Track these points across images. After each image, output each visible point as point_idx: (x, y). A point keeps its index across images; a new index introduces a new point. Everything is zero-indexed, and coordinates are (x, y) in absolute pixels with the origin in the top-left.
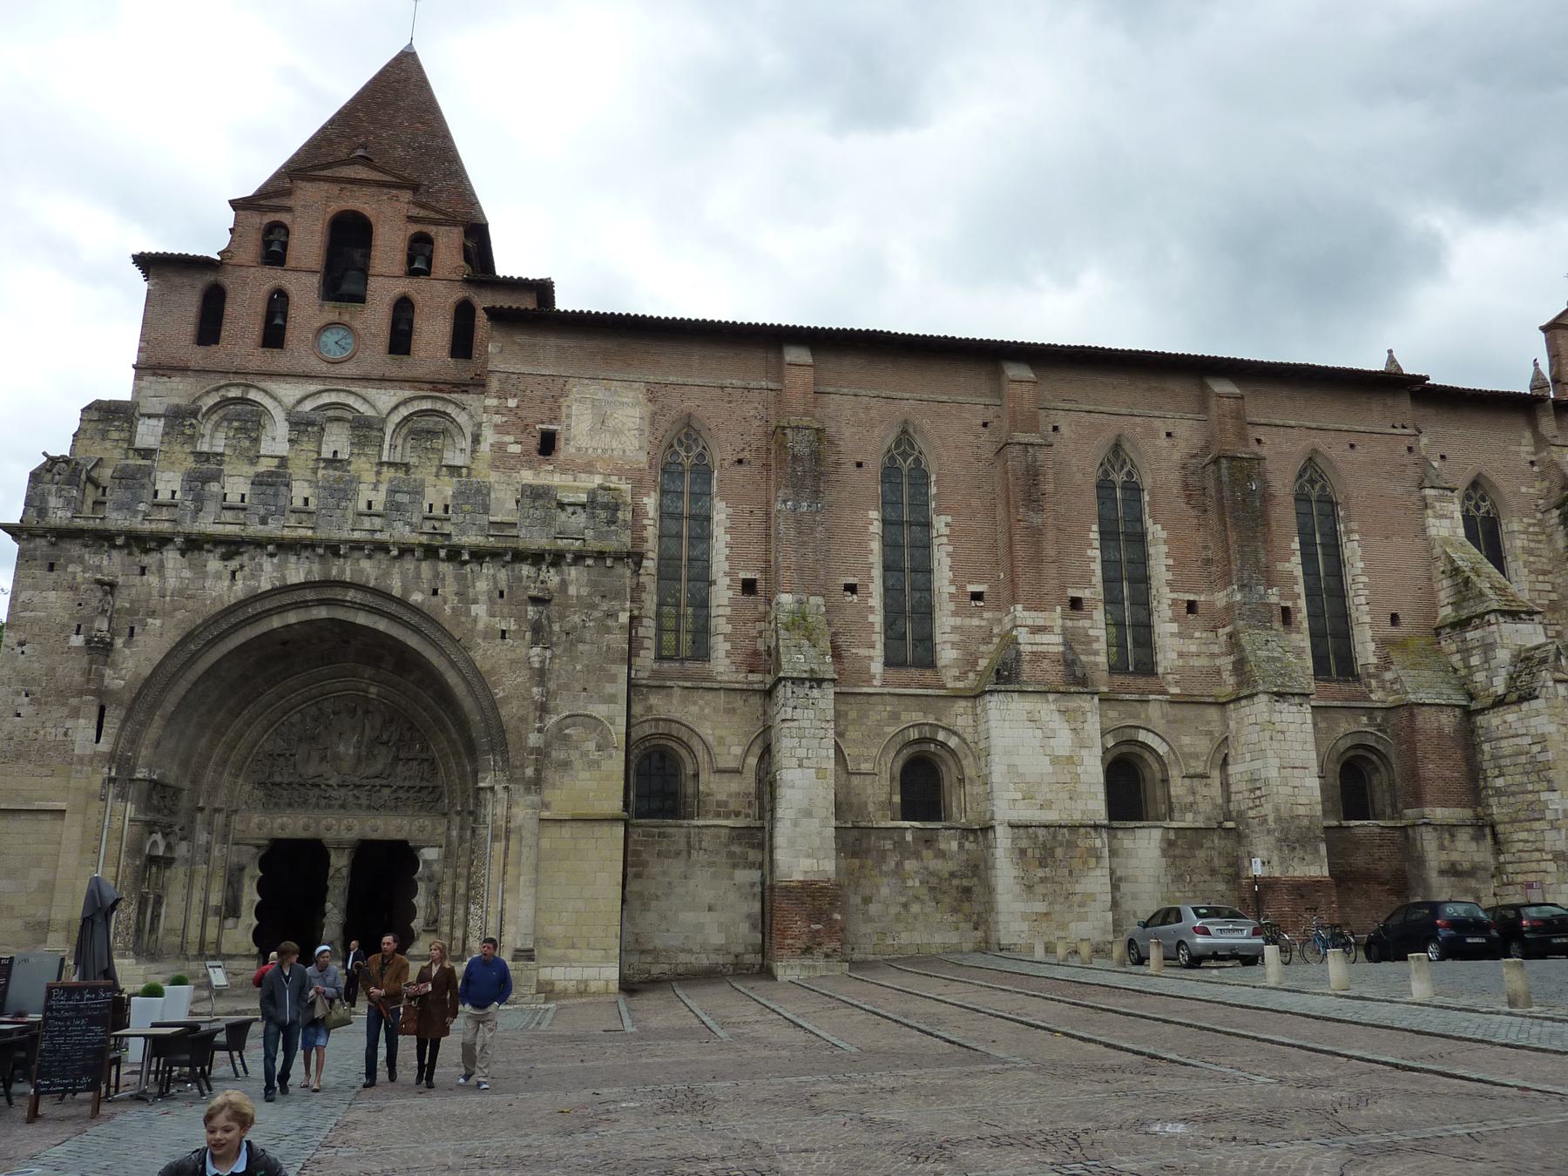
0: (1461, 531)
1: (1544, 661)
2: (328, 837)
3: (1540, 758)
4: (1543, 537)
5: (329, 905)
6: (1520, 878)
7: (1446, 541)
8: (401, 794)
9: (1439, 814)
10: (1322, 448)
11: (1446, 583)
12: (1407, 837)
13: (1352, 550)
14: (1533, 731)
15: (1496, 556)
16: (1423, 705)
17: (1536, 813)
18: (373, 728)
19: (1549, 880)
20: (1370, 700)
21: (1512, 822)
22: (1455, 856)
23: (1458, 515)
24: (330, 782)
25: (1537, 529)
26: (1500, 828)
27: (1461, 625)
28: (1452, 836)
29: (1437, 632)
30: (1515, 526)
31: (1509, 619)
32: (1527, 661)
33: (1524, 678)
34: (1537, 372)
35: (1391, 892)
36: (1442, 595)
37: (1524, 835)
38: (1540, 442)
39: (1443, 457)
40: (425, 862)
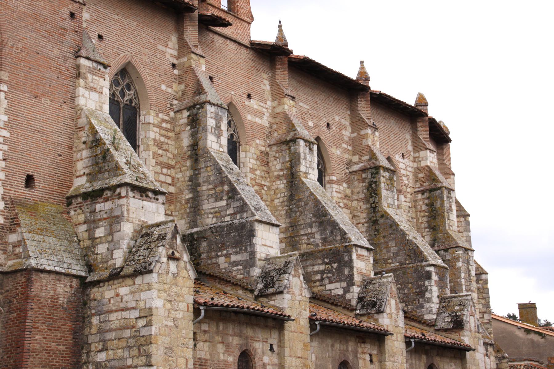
1: (162, 237)
3: (144, 332)
4: (172, 134)
7: (92, 113)
11: (85, 153)
14: (142, 305)
15: (131, 133)
23: (106, 92)
25: (168, 126)
29: (69, 200)
30: (152, 119)
31: (138, 195)
32: (146, 235)
33: (142, 252)
38: (183, 48)
39: (100, 37)
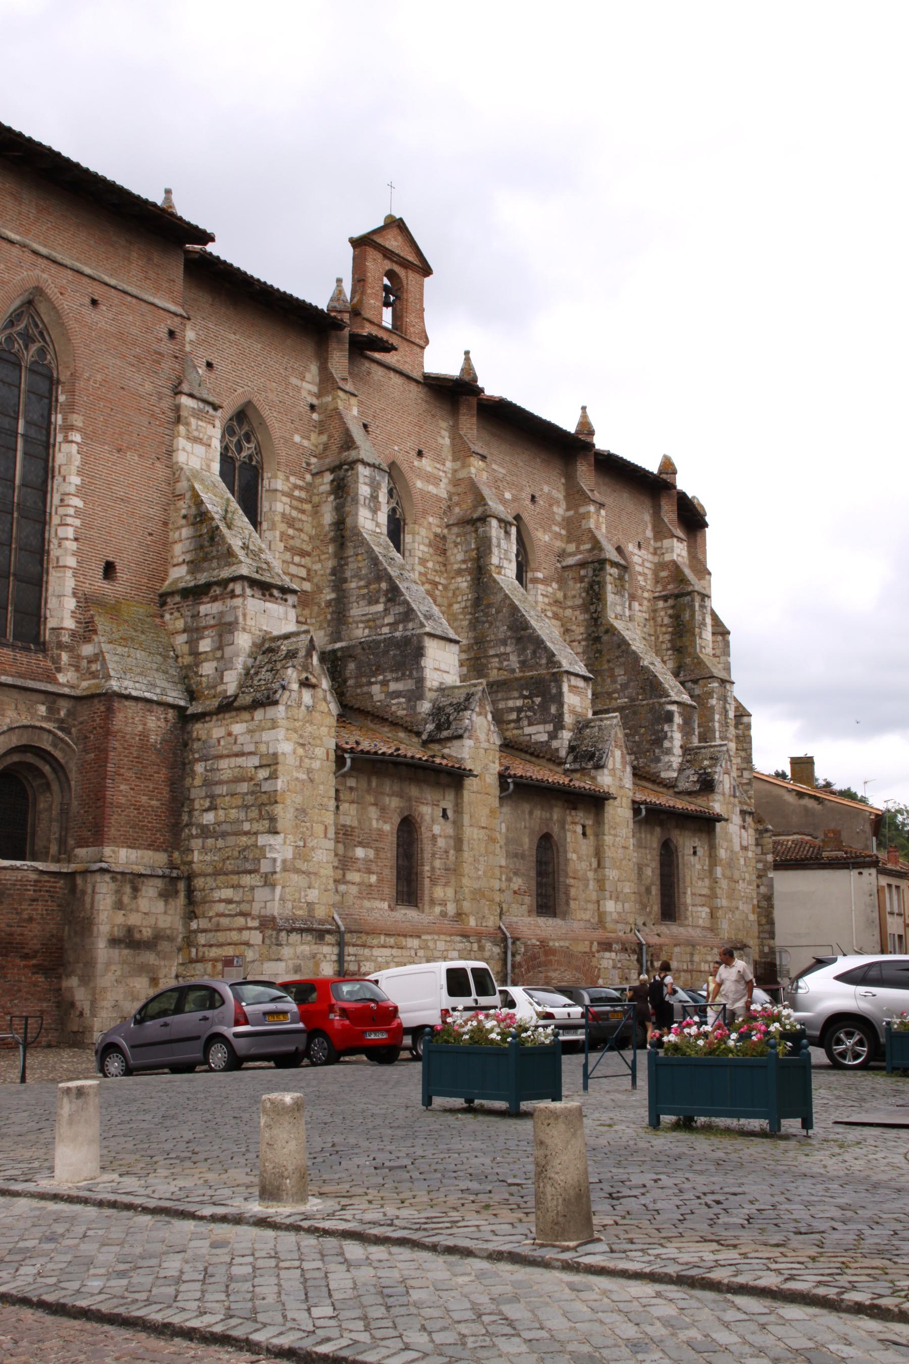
0: (216, 467)
1: (292, 655)
3: (266, 787)
4: (307, 507)
6: (214, 952)
7: (196, 474)
9: (123, 857)
10: (51, 291)
11: (186, 532)
12: (73, 889)
13: (68, 455)
14: (263, 749)
15: (251, 505)
16: (129, 697)
17: (249, 862)
19: (250, 955)
20: (54, 681)
21: (216, 873)
22: (134, 919)
23: (216, 444)
25: (303, 495)
26: (199, 882)
27: (196, 593)
28: (136, 890)
30: (279, 484)
31: (258, 594)
34: (340, 291)
35: (38, 969)
36: (178, 549)
37: (227, 893)
38: (327, 382)
39: (209, 365)
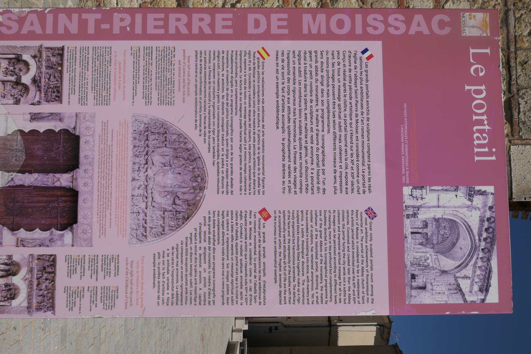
2: (80, 172)
5: (36, 175)
8: (142, 216)
18: (184, 193)
24: (149, 170)
40: (63, 235)
